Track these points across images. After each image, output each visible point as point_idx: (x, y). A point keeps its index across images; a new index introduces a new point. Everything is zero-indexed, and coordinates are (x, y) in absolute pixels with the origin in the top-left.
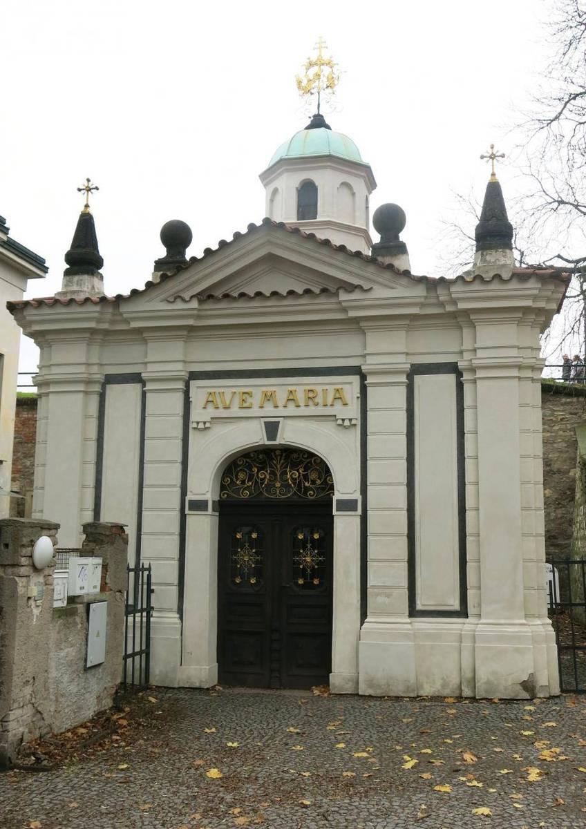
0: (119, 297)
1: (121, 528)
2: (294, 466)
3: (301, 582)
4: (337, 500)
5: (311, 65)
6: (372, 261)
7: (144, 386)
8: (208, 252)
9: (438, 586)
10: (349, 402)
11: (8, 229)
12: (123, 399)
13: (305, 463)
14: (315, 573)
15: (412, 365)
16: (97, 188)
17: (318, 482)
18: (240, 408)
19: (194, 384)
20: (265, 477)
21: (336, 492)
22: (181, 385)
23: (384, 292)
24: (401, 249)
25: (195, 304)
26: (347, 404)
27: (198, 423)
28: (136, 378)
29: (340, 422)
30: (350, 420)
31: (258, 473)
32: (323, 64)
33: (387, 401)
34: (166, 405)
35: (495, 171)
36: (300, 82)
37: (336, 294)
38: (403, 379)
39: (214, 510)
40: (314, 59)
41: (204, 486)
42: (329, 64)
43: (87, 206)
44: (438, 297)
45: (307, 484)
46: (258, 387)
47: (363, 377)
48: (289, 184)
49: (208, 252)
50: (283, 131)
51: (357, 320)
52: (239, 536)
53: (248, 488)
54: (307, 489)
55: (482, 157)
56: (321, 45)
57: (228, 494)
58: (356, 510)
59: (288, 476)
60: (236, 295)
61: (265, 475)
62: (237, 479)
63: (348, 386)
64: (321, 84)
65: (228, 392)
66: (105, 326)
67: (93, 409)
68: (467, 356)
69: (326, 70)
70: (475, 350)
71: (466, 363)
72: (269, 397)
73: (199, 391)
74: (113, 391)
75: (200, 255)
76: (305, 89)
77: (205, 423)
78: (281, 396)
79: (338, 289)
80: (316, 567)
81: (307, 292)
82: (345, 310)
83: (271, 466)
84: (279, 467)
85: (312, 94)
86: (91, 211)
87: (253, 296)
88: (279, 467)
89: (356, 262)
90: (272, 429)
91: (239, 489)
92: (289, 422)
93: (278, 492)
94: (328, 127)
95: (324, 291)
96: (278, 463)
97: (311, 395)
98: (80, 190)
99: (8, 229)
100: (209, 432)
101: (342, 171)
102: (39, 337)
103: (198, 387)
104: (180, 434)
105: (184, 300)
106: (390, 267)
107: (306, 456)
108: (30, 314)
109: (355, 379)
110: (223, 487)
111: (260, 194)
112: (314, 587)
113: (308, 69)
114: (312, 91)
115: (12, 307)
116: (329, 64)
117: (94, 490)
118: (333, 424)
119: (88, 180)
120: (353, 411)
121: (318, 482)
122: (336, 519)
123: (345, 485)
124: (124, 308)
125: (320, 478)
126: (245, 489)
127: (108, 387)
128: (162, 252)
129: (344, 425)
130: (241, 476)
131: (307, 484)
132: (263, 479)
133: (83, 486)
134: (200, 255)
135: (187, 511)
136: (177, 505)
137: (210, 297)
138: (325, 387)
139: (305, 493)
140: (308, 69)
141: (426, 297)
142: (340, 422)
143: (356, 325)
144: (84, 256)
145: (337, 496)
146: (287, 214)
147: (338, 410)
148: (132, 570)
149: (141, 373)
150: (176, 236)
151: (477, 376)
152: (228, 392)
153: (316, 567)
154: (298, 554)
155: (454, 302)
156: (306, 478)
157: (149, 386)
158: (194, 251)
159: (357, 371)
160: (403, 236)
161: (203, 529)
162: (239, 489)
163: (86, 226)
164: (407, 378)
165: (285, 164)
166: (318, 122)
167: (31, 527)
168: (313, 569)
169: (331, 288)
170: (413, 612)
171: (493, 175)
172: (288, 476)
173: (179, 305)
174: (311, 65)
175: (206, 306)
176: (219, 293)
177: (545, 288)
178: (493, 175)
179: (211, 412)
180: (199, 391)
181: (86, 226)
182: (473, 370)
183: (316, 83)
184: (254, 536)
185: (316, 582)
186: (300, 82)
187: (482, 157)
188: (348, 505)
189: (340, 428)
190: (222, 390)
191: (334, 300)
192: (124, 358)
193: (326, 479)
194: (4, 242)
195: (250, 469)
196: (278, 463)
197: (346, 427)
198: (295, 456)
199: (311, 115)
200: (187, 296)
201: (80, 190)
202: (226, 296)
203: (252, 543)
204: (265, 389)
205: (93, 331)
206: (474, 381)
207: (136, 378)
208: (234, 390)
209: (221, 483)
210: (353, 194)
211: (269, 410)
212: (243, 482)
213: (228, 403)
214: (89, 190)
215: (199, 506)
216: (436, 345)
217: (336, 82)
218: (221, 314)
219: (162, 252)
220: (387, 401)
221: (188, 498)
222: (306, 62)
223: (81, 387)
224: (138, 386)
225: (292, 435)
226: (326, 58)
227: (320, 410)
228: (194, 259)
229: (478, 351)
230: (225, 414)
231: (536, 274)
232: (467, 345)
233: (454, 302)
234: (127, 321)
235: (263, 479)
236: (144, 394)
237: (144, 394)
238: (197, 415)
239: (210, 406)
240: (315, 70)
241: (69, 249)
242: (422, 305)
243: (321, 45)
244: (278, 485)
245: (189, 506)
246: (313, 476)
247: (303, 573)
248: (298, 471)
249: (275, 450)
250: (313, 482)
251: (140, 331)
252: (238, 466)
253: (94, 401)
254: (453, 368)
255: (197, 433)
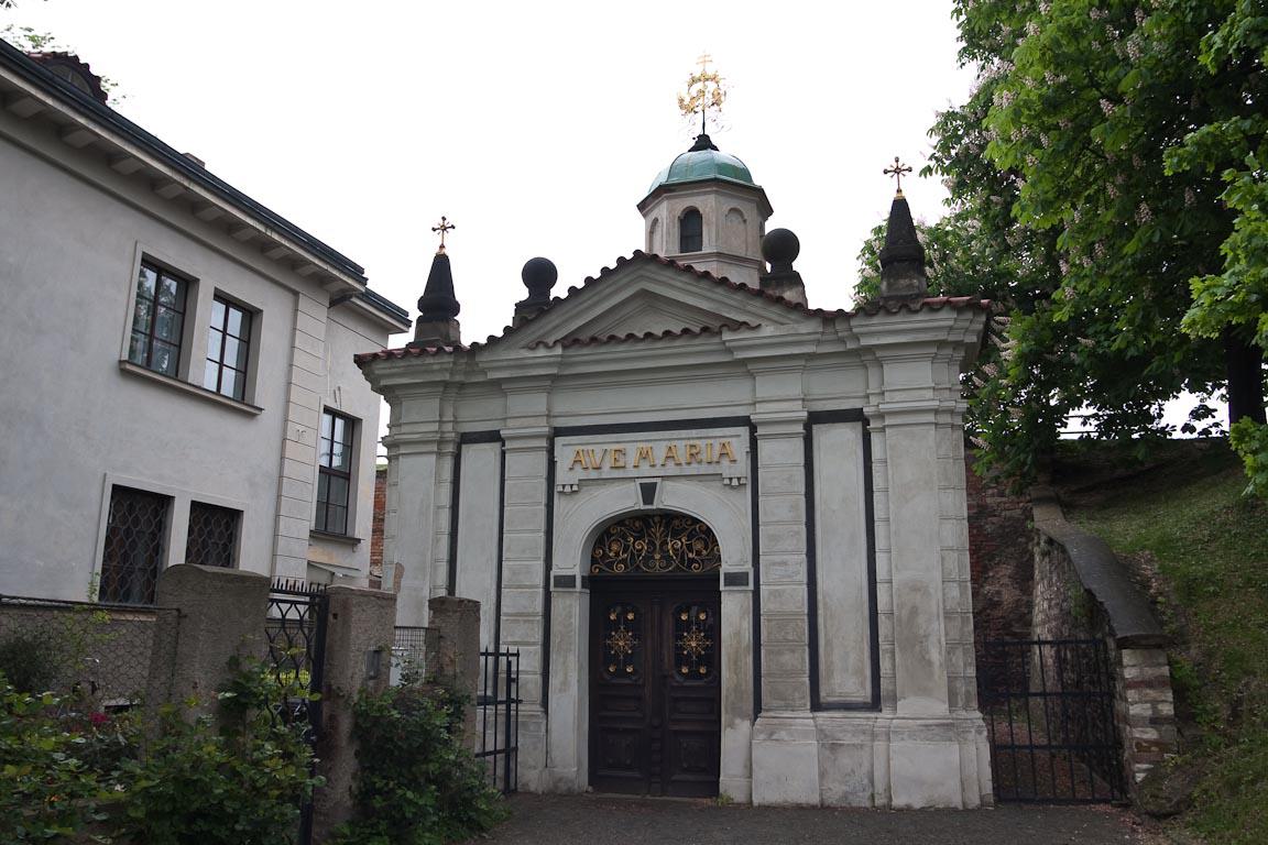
0: (475, 345)
1: (476, 605)
2: (676, 534)
3: (685, 670)
4: (555, 577)
5: (694, 81)
6: (759, 294)
7: (503, 445)
8: (572, 290)
9: (847, 680)
10: (737, 457)
11: (367, 279)
12: (479, 460)
13: (688, 532)
14: (701, 660)
15: (810, 413)
16: (453, 227)
17: (704, 552)
18: (612, 467)
19: (559, 441)
20: (643, 547)
21: (723, 564)
22: (544, 443)
23: (771, 329)
24: (796, 280)
25: (559, 351)
26: (735, 461)
27: (564, 486)
28: (493, 437)
29: (727, 482)
30: (739, 479)
31: (634, 543)
32: (707, 80)
33: (781, 455)
34: (527, 467)
35: (901, 188)
36: (682, 101)
37: (720, 333)
38: (800, 428)
39: (583, 586)
40: (697, 75)
41: (571, 560)
42: (714, 79)
43: (442, 247)
44: (851, 329)
45: (690, 555)
46: (632, 445)
47: (753, 428)
48: (666, 211)
49: (572, 290)
50: (661, 150)
51: (744, 362)
52: (612, 617)
53: (623, 561)
54: (692, 561)
55: (886, 172)
56: (705, 59)
57: (600, 569)
58: (747, 584)
59: (669, 547)
60: (641, 335)
61: (642, 545)
62: (610, 550)
63: (734, 439)
64: (706, 101)
65: (598, 449)
66: (458, 378)
67: (447, 475)
68: (874, 400)
69: (711, 86)
70: (883, 393)
71: (873, 409)
72: (644, 456)
73: (565, 450)
74: (825, 436)
75: (564, 294)
76: (688, 108)
77: (571, 486)
78: (660, 451)
79: (721, 327)
80: (703, 652)
81: (686, 331)
82: (730, 351)
83: (649, 535)
84: (658, 534)
85: (696, 112)
86: (446, 251)
87: (679, 333)
88: (658, 534)
89: (739, 296)
90: (648, 491)
91: (613, 563)
92: (669, 484)
93: (658, 566)
94: (715, 148)
95: (705, 330)
96: (658, 531)
97: (694, 451)
98: (434, 230)
99: (367, 279)
100: (576, 497)
101: (732, 196)
102: (388, 392)
103: (564, 445)
104: (543, 499)
105: (547, 346)
106: (780, 300)
107: (689, 523)
108: (380, 368)
109: (744, 431)
110: (594, 561)
111: (639, 224)
112: (701, 676)
113: (690, 86)
114: (696, 109)
115: (360, 361)
116: (714, 79)
117: (815, 799)
118: (719, 484)
119: (444, 219)
120: (742, 468)
121: (704, 552)
122: (724, 597)
123: (733, 556)
124: (483, 358)
125: (706, 548)
126: (620, 562)
127: (464, 447)
128: (523, 293)
129: (733, 485)
130: (615, 547)
131: (690, 555)
132: (641, 550)
133: (436, 561)
134: (564, 294)
135: (552, 589)
136: (540, 580)
137: (576, 342)
138: (709, 441)
139: (689, 567)
140: (690, 86)
141: (823, 333)
142: (727, 482)
143: (744, 368)
144: (440, 298)
145: (725, 568)
146: (666, 248)
147: (725, 468)
148: (491, 654)
149: (499, 431)
150: (539, 274)
151: (886, 423)
152: (598, 449)
153: (703, 652)
154: (681, 637)
155: (856, 337)
156: (690, 548)
157: (508, 445)
158: (559, 291)
159: (744, 421)
160: (797, 265)
161: (573, 611)
162: (613, 563)
163: (441, 266)
164: (805, 429)
165: (661, 192)
166: (704, 143)
167: (362, 595)
168: (699, 656)
169: (713, 327)
170: (817, 706)
171: (899, 191)
172: (669, 547)
173: (542, 352)
174: (694, 81)
175: (571, 352)
176: (584, 337)
177: (962, 317)
178: (899, 191)
179: (579, 474)
180: (565, 450)
181: (441, 266)
182: (881, 416)
183: (700, 101)
184: (630, 616)
185: (703, 670)
186: (682, 101)
187: (886, 172)
188: (736, 579)
189: (727, 488)
190: (590, 447)
191: (716, 340)
192: (478, 414)
193: (712, 549)
194: (362, 294)
195: (625, 538)
196: (658, 531)
197: (732, 487)
198: (676, 522)
199: (696, 135)
200: (550, 341)
201: (434, 230)
202: (594, 340)
203: (629, 625)
204: (641, 445)
205: (446, 385)
206: (883, 429)
207: (493, 437)
208: (605, 447)
209: (592, 557)
210: (745, 221)
211: (645, 470)
212: (617, 554)
213: (598, 461)
214: (444, 229)
215: (566, 582)
216: (839, 388)
217: (723, 98)
218: (589, 360)
219: (523, 293)
220: (781, 455)
221: (552, 574)
222: (688, 78)
223: (931, 418)
224: (497, 445)
225: (672, 498)
226: (710, 73)
227: (704, 469)
228: (556, 298)
229: (886, 394)
230: (594, 475)
231: (951, 302)
232: (873, 388)
233: (856, 337)
234: (484, 372)
235: (641, 550)
236: (503, 454)
237: (503, 454)
238: (562, 476)
239: (578, 467)
240: (699, 86)
241: (422, 294)
242: (819, 342)
243: (705, 59)
244: (657, 556)
245: (554, 583)
246: (699, 546)
247: (686, 660)
248: (680, 540)
249: (654, 516)
250: (699, 553)
251: (497, 383)
252: (607, 534)
253: (448, 463)
254: (855, 416)
255: (563, 498)
